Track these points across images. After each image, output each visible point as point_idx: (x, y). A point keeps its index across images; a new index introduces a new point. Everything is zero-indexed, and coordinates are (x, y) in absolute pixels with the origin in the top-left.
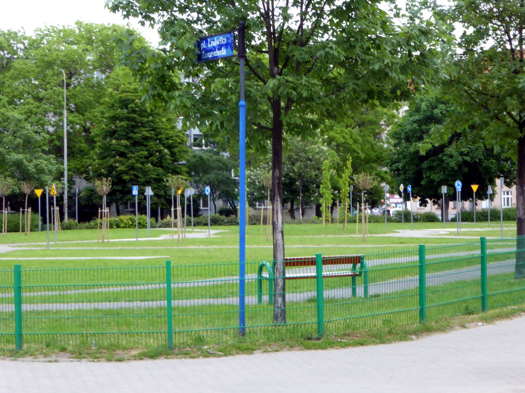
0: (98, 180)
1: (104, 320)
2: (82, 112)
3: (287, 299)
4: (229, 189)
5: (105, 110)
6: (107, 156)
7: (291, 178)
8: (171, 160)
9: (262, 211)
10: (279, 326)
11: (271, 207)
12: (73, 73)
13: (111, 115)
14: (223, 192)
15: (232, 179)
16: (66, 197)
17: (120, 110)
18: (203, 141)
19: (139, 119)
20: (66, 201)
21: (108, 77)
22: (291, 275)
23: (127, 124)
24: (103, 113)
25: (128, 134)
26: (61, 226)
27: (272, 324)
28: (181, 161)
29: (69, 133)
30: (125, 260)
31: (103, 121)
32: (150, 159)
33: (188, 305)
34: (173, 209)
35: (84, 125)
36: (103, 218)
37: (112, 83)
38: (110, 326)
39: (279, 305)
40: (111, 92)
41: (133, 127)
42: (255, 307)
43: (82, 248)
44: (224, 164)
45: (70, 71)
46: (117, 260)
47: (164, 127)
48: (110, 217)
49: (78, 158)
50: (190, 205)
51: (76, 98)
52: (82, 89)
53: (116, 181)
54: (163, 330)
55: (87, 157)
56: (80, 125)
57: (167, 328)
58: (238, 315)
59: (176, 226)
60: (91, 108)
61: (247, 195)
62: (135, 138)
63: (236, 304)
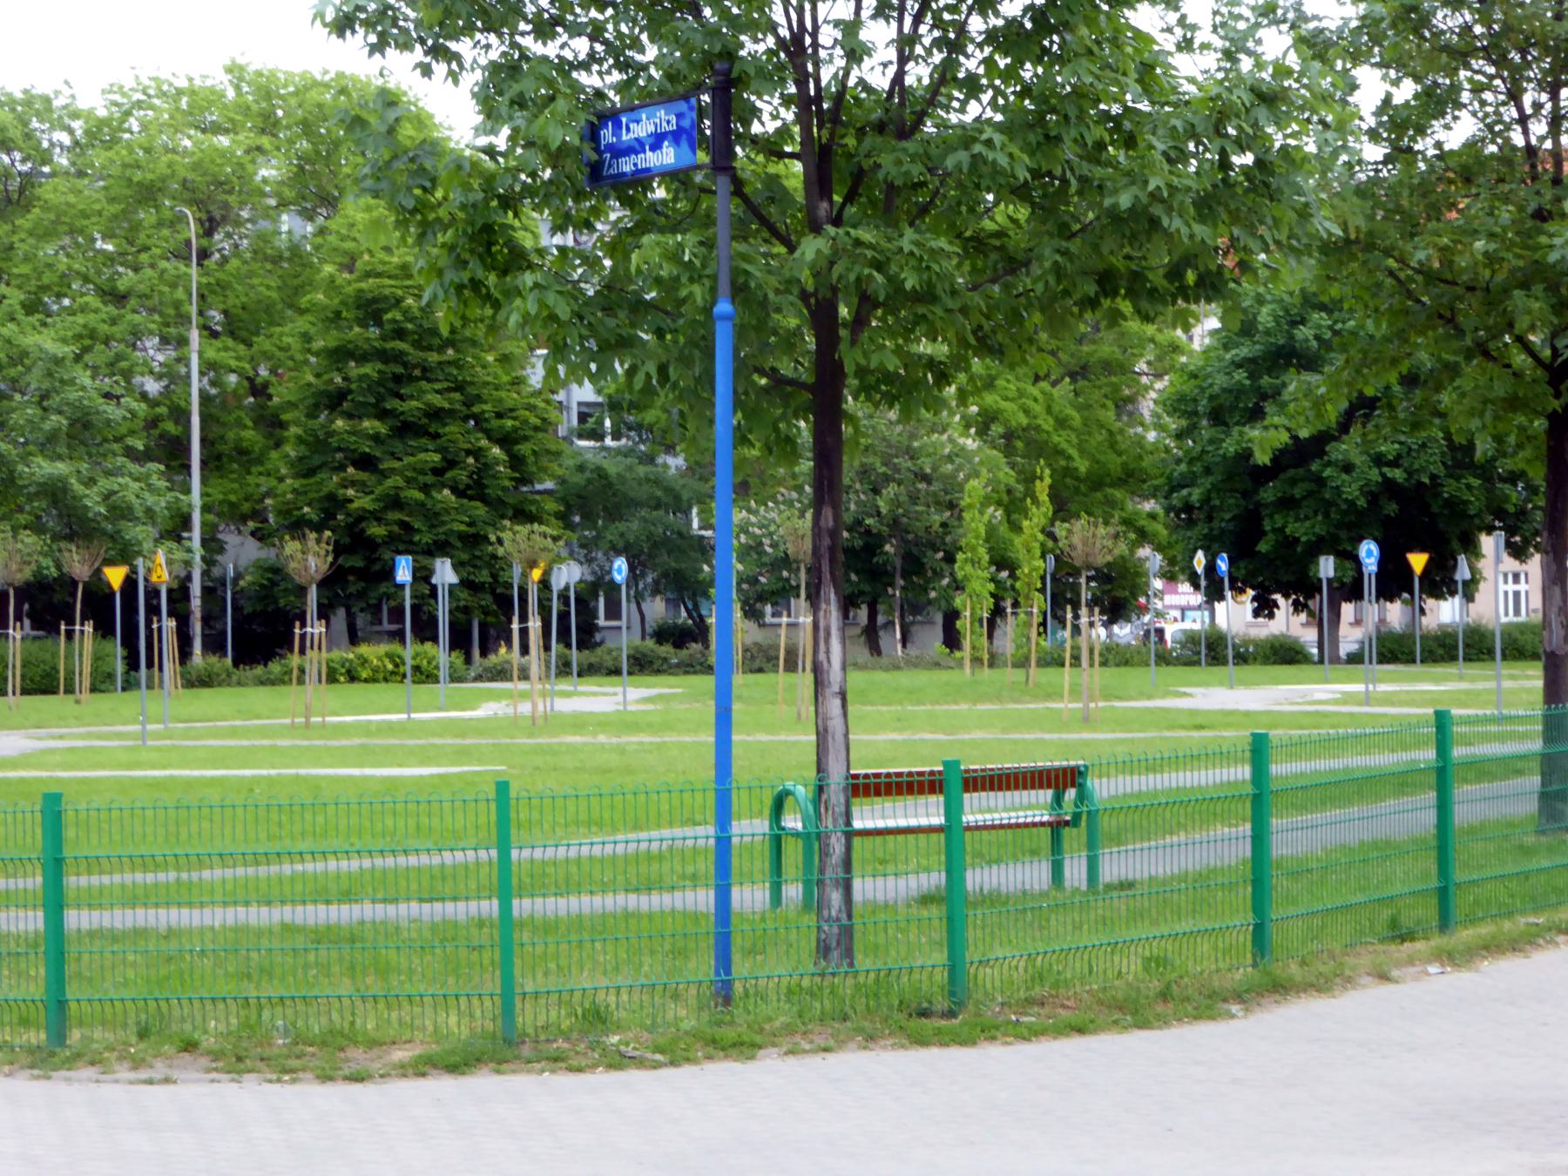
0: (293, 538)
1: (311, 957)
2: (244, 334)
3: (857, 896)
4: (683, 566)
5: (312, 330)
6: (320, 467)
7: (868, 532)
8: (512, 479)
9: (783, 632)
10: (833, 974)
11: (809, 620)
12: (218, 217)
13: (332, 344)
14: (665, 575)
15: (692, 537)
16: (196, 589)
17: (357, 329)
18: (608, 423)
19: (414, 355)
20: (196, 603)
21: (321, 232)
22: (870, 824)
23: (379, 372)
24: (307, 338)
25: (384, 400)
26: (182, 676)
27: (811, 969)
28: (541, 481)
29: (205, 399)
30: (372, 777)
31: (306, 362)
32: (449, 475)
33: (562, 913)
34: (515, 626)
35: (251, 374)
36: (308, 651)
37: (335, 249)
38: (328, 976)
39: (834, 913)
40: (331, 276)
41: (397, 379)
42: (763, 919)
43: (245, 743)
44: (669, 490)
45: (208, 212)
46: (351, 777)
47: (489, 379)
48: (329, 650)
49: (232, 472)
50: (569, 613)
51: (228, 293)
52: (246, 267)
53: (347, 540)
54: (488, 988)
55: (261, 469)
56: (240, 375)
57: (498, 982)
58: (712, 941)
59: (524, 675)
60: (272, 323)
61: (738, 584)
62: (402, 413)
63: (704, 910)
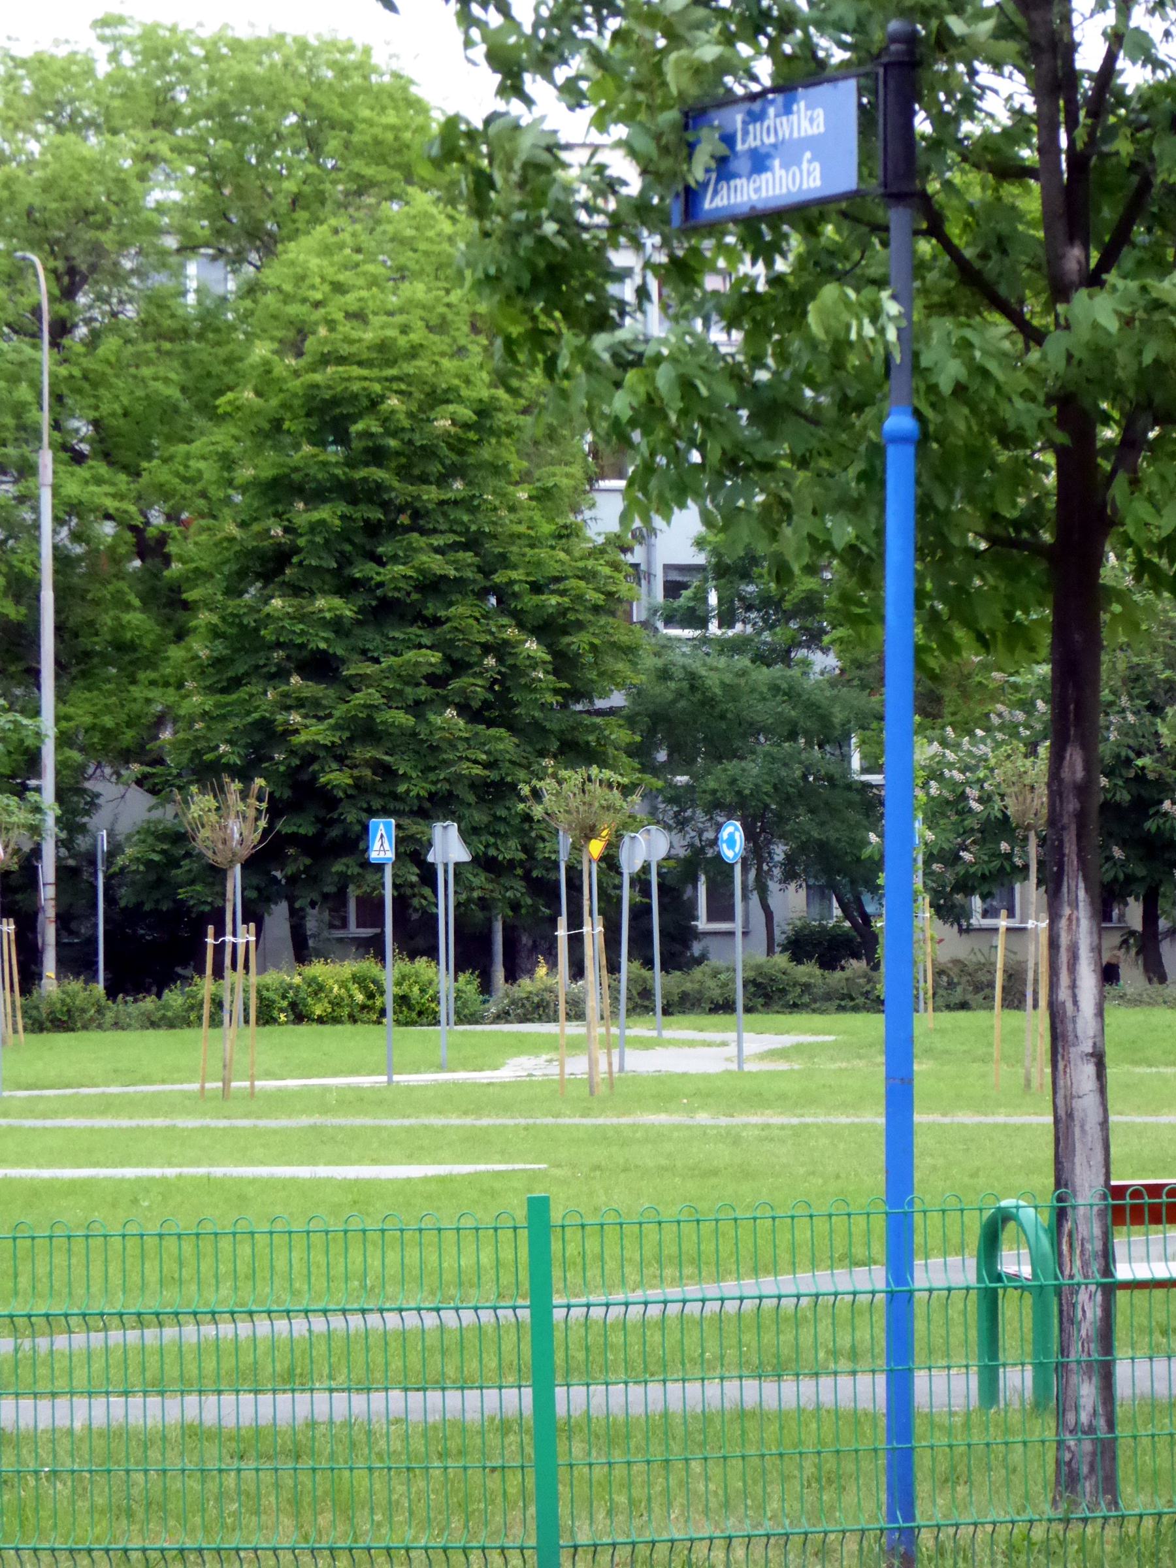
0: (202, 791)
1: (230, 1480)
2: (126, 456)
3: (1122, 1387)
4: (833, 835)
5: (237, 450)
6: (247, 674)
7: (1141, 777)
8: (556, 691)
9: (1000, 941)
10: (1085, 1520)
11: (1044, 924)
12: (84, 267)
13: (267, 473)
14: (803, 848)
15: (849, 787)
16: (47, 871)
17: (307, 449)
18: (713, 599)
19: (401, 491)
20: (47, 893)
21: (252, 290)
22: (1142, 1272)
23: (343, 517)
24: (227, 462)
25: (350, 563)
26: (25, 1013)
27: (1049, 1512)
28: (604, 694)
29: (62, 560)
30: (329, 1180)
31: (227, 500)
32: (454, 684)
33: (637, 1410)
34: (562, 932)
35: (139, 521)
36: (228, 972)
37: (274, 317)
38: (257, 1513)
39: (1084, 1418)
40: (266, 363)
41: (372, 530)
42: (967, 1425)
43: (125, 1123)
44: (812, 708)
45: (67, 259)
46: (294, 1180)
47: (522, 529)
48: (262, 970)
49: (108, 680)
50: (648, 909)
51: (102, 391)
52: (130, 349)
53: (287, 793)
54: (517, 1535)
55: (153, 675)
56: (120, 524)
57: (532, 1526)
58: (882, 1461)
59: (576, 1012)
60: (170, 439)
61: (927, 863)
62: (380, 585)
63: (869, 1407)
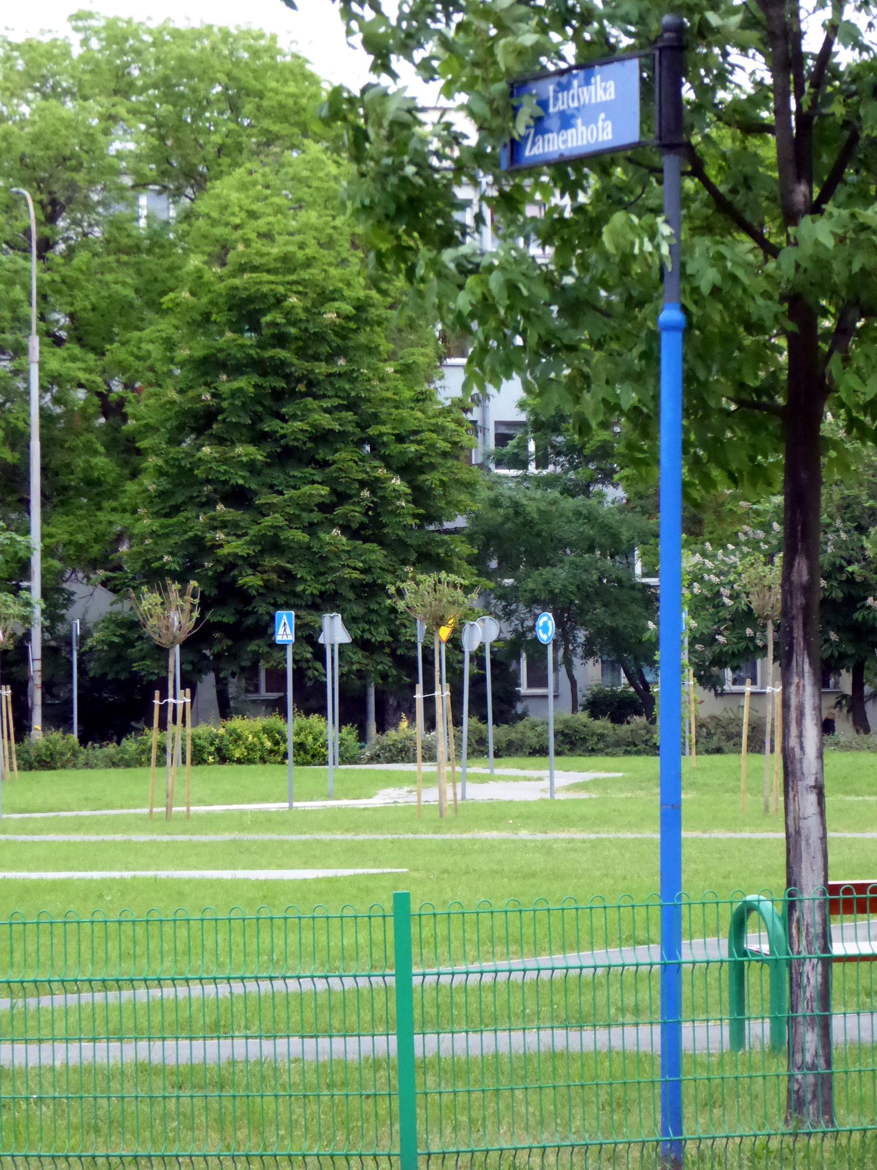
0: (151, 590)
1: (172, 1105)
2: (94, 340)
3: (837, 1035)
4: (621, 623)
5: (176, 336)
6: (184, 503)
7: (851, 580)
8: (415, 516)
9: (746, 702)
10: (809, 1134)
11: (779, 690)
12: (62, 200)
13: (199, 353)
14: (599, 633)
15: (633, 587)
16: (35, 650)
17: (229, 335)
18: (532, 447)
19: (299, 366)
20: (35, 667)
21: (188, 216)
22: (852, 949)
23: (256, 386)
24: (170, 344)
25: (261, 420)
26: (19, 756)
27: (783, 1128)
28: (451, 518)
29: (46, 418)
30: (245, 880)
31: (170, 373)
32: (339, 511)
33: (475, 1052)
34: (419, 696)
35: (103, 388)
36: (170, 725)
37: (205, 237)
38: (192, 1129)
39: (808, 1058)
40: (199, 271)
41: (278, 395)
42: (721, 1063)
43: (93, 838)
44: (605, 528)
45: (50, 193)
46: (219, 881)
47: (389, 394)
48: (195, 724)
49: (81, 508)
50: (483, 678)
51: (76, 292)
52: (97, 260)
53: (214, 592)
54: (385, 1145)
55: (114, 504)
56: (89, 391)
57: (397, 1139)
58: (658, 1090)
59: (430, 755)
60: (127, 327)
61: (691, 644)
62: (284, 436)
63: (648, 1050)
